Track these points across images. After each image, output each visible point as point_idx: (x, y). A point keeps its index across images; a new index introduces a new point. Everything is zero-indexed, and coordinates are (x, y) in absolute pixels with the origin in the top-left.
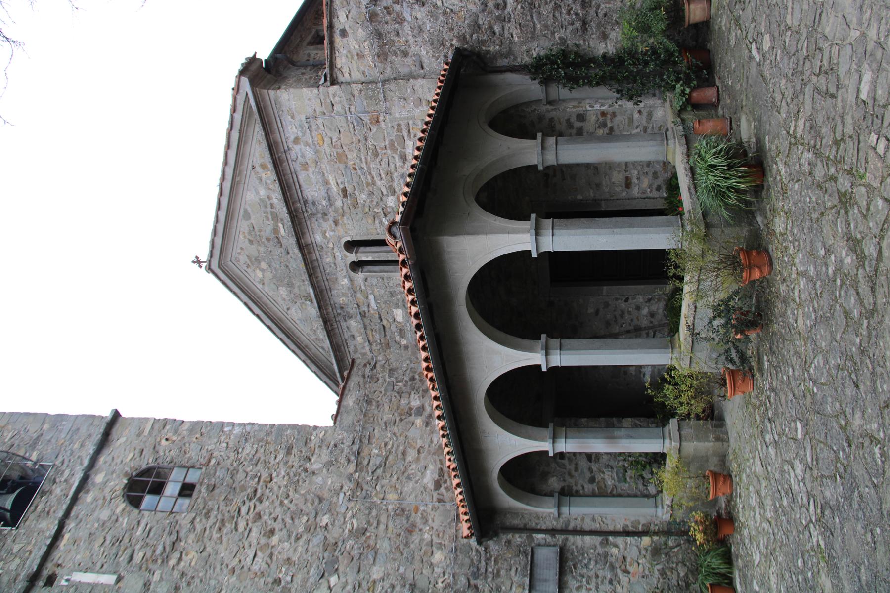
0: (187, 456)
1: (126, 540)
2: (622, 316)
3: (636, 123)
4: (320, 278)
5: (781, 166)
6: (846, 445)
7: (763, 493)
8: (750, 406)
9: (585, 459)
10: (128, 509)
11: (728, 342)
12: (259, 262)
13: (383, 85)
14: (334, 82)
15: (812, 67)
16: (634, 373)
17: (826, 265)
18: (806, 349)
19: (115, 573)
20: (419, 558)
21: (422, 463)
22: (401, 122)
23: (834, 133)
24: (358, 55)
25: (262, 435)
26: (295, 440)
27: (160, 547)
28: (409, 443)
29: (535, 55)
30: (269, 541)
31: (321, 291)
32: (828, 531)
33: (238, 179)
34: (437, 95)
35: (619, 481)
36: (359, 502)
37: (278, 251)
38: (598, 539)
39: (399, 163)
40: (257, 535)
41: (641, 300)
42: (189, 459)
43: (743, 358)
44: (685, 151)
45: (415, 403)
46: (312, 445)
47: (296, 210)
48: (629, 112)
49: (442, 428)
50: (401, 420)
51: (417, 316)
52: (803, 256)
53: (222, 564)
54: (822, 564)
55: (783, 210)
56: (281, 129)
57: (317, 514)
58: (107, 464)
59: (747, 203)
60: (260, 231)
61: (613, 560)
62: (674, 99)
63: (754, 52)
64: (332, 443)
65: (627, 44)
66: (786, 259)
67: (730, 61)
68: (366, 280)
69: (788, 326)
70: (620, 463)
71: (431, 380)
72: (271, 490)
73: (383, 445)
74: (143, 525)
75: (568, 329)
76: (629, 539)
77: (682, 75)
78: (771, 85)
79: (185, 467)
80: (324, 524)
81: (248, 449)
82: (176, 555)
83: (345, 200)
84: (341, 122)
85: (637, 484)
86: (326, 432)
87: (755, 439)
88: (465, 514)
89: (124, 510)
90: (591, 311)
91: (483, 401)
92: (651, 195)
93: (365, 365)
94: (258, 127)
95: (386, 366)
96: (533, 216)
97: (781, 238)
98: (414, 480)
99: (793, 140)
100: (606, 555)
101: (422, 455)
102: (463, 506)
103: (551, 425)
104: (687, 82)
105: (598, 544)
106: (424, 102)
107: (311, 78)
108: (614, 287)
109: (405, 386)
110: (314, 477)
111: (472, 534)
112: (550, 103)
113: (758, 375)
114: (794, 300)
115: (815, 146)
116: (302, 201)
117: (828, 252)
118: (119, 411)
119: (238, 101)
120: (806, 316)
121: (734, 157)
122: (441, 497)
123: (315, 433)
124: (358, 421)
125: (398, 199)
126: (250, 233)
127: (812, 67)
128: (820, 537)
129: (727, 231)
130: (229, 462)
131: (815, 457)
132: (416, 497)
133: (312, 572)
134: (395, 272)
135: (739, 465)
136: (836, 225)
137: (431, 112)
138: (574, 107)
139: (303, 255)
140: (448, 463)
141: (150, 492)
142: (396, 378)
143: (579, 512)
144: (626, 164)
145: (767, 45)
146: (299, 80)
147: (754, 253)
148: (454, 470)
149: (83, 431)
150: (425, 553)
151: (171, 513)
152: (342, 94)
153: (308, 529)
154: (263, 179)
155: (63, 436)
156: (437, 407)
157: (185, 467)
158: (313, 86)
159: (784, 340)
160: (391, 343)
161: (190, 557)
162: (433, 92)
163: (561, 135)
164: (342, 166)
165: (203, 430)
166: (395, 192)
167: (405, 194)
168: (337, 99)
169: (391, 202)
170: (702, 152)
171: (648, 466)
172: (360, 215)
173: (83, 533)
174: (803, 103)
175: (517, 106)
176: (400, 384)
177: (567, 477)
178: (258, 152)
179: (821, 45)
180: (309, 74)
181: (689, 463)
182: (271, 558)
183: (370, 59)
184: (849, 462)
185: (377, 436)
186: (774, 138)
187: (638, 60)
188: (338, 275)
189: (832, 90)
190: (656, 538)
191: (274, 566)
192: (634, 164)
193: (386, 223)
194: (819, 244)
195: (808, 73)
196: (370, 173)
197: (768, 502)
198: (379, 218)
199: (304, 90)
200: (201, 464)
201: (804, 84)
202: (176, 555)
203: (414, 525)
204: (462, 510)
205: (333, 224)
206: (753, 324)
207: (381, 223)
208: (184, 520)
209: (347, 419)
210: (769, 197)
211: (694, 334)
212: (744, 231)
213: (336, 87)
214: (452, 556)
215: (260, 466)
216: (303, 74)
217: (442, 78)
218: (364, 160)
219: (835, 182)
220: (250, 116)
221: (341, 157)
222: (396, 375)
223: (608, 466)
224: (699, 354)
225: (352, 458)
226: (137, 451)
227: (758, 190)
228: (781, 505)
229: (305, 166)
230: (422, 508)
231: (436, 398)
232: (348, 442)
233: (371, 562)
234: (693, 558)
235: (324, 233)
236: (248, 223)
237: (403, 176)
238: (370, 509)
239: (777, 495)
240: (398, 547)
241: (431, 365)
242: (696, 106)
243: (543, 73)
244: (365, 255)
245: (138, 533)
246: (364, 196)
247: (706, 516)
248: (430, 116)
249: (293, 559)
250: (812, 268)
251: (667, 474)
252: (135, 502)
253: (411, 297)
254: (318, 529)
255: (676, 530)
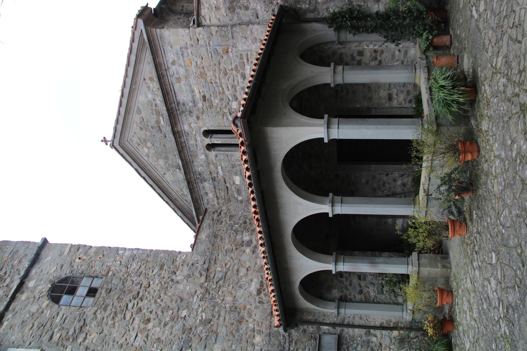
0: (93, 269)
1: (48, 325)
2: (384, 185)
3: (396, 58)
4: (186, 154)
5: (487, 87)
6: (521, 265)
7: (472, 301)
8: (464, 244)
9: (357, 278)
10: (50, 304)
11: (450, 201)
12: (146, 143)
13: (231, 28)
14: (199, 25)
15: (508, 23)
16: (391, 223)
17: (512, 151)
18: (498, 205)
19: (39, 348)
20: (245, 339)
21: (250, 277)
22: (242, 53)
23: (519, 66)
24: (216, 7)
25: (144, 256)
26: (167, 260)
27: (72, 330)
28: (241, 264)
29: (332, 11)
30: (147, 327)
31: (187, 163)
32: (510, 323)
33: (134, 87)
34: (267, 36)
35: (378, 294)
36: (207, 301)
37: (159, 135)
38: (363, 331)
39: (240, 80)
40: (138, 322)
41: (397, 175)
42: (94, 271)
43: (460, 212)
44: (427, 77)
45: (246, 238)
46: (177, 264)
47: (172, 109)
48: (392, 51)
49: (263, 252)
50: (237, 249)
51: (249, 178)
52: (498, 145)
53: (114, 341)
54: (508, 346)
55: (487, 116)
56: (164, 55)
57: (179, 309)
58: (38, 274)
59: (465, 111)
60: (147, 122)
61: (373, 345)
62: (422, 43)
63: (474, 13)
64: (191, 263)
65: (392, 5)
66: (488, 147)
67: (459, 18)
68: (216, 156)
69: (489, 191)
70: (380, 282)
71: (257, 220)
72: (149, 293)
73: (224, 265)
74: (60, 315)
75: (347, 190)
76: (384, 332)
77: (427, 27)
78: (483, 34)
79: (91, 277)
80: (183, 316)
81: (135, 266)
82: (83, 335)
83: (204, 103)
84: (203, 52)
85: (390, 296)
86: (187, 255)
87: (467, 266)
88: (277, 311)
89: (48, 305)
90: (363, 181)
91: (290, 236)
92: (405, 106)
93: (214, 213)
94: (149, 53)
95: (228, 213)
96: (326, 116)
97: (485, 134)
98: (244, 288)
99: (494, 70)
100: (369, 342)
101: (250, 272)
102: (275, 305)
103: (334, 253)
104: (431, 32)
105: (363, 334)
106: (258, 40)
107: (184, 21)
108: (379, 166)
109: (240, 227)
110: (178, 285)
111: (281, 325)
112: (340, 43)
113: (469, 223)
114: (492, 174)
115: (507, 74)
116: (176, 103)
117: (513, 142)
118: (47, 238)
119: (136, 35)
120: (499, 184)
121: (458, 80)
122: (261, 300)
123: (179, 256)
124: (208, 249)
125: (240, 103)
126: (141, 123)
127: (508, 23)
128: (506, 328)
129: (451, 129)
130: (121, 273)
131: (503, 275)
132: (245, 299)
133: (174, 347)
134: (236, 151)
135: (457, 284)
136: (518, 125)
137: (263, 47)
138: (356, 46)
139: (175, 138)
140: (266, 276)
141: (66, 294)
142: (234, 222)
143: (351, 312)
144: (390, 84)
145: (482, 8)
146: (176, 23)
147: (468, 143)
148: (270, 280)
149: (21, 252)
150: (249, 336)
151: (81, 307)
152: (204, 33)
153: (172, 319)
154: (151, 88)
155: (6, 255)
156: (261, 238)
157: (91, 277)
158: (185, 27)
159: (486, 199)
160: (232, 199)
161: (92, 336)
162: (264, 34)
163: (347, 64)
164: (203, 81)
165: (105, 253)
166: (237, 99)
167: (245, 99)
168: (201, 36)
169: (234, 105)
170: (437, 78)
171: (397, 284)
172: (214, 114)
173: (18, 321)
174: (502, 46)
175: (319, 45)
176: (237, 226)
177: (344, 290)
178: (148, 69)
179: (514, 9)
180: (183, 19)
181: (424, 282)
182: (147, 338)
183: (223, 10)
184: (523, 276)
185: (220, 259)
186: (483, 69)
187: (399, 16)
188: (199, 152)
189: (520, 38)
190: (402, 332)
191: (148, 343)
192: (395, 84)
193: (231, 119)
194: (507, 137)
195: (505, 27)
196: (221, 86)
197: (475, 307)
198: (226, 115)
199: (180, 29)
200: (102, 275)
201: (503, 34)
202: (83, 335)
203: (243, 318)
204: (274, 308)
205: (196, 119)
206: (466, 190)
207: (228, 119)
208: (89, 312)
209: (201, 247)
210: (479, 107)
211: (428, 195)
212: (463, 129)
213: (200, 29)
214: (267, 338)
215: (142, 277)
216: (179, 19)
217: (270, 25)
218: (217, 77)
219: (518, 97)
220: (143, 45)
221: (203, 75)
222: (234, 219)
223: (371, 283)
224: (431, 209)
225: (203, 273)
226: (59, 266)
227: (473, 102)
228: (483, 308)
229: (179, 80)
230: (248, 307)
231: (260, 232)
232: (201, 263)
233: (214, 342)
234: (426, 346)
235: (190, 125)
236: (140, 116)
237: (243, 88)
238: (214, 306)
239: (480, 302)
240: (232, 332)
241: (258, 210)
242: (436, 48)
243: (336, 24)
244: (217, 140)
245: (57, 321)
246: (217, 101)
247: (435, 317)
248: (262, 49)
249: (162, 339)
250: (503, 153)
251: (410, 289)
252: (56, 300)
253: (246, 166)
254: (180, 319)
255: (414, 327)
